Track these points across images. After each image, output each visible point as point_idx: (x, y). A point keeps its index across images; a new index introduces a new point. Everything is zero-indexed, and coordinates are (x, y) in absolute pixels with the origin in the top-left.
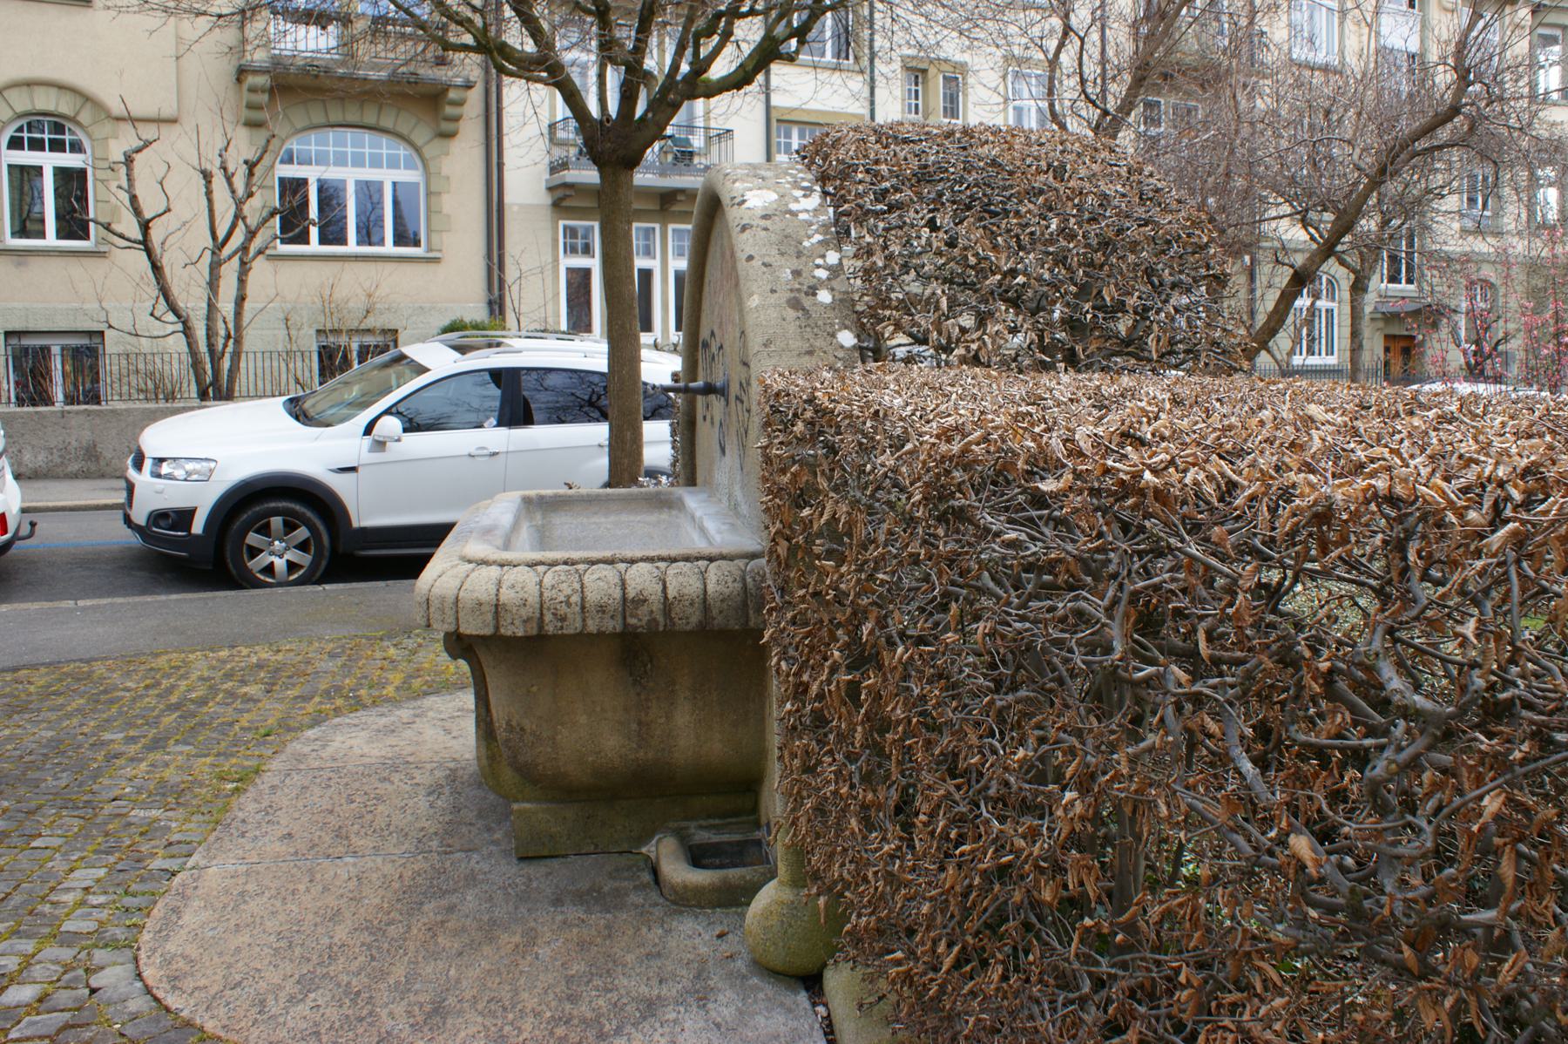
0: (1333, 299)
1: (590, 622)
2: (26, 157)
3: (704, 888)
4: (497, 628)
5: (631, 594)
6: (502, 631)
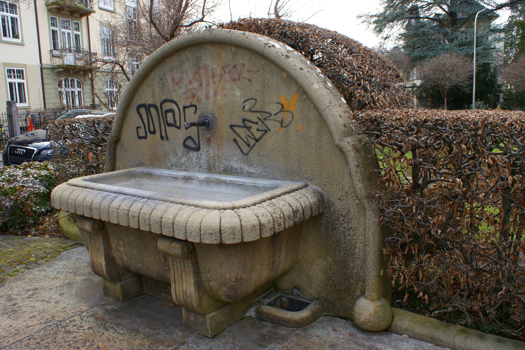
0: (80, 88)
1: (286, 224)
2: (12, 80)
3: (309, 317)
4: (242, 238)
5: (295, 209)
6: (202, 241)
